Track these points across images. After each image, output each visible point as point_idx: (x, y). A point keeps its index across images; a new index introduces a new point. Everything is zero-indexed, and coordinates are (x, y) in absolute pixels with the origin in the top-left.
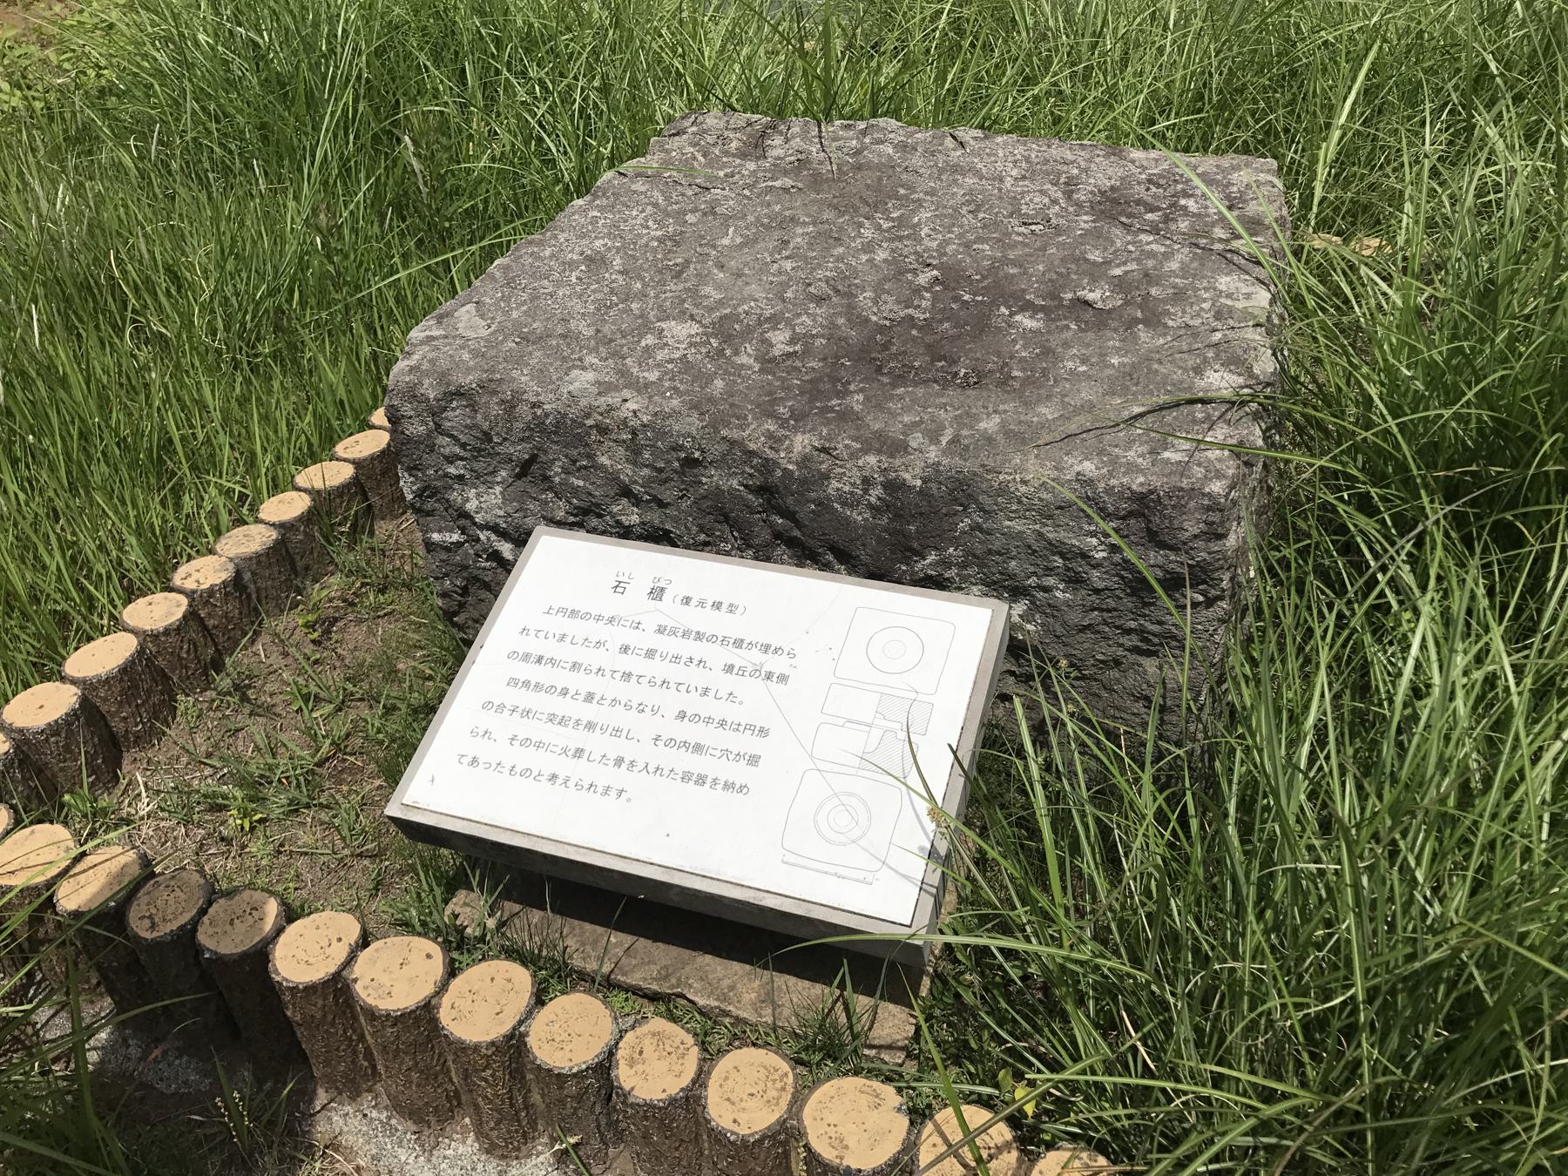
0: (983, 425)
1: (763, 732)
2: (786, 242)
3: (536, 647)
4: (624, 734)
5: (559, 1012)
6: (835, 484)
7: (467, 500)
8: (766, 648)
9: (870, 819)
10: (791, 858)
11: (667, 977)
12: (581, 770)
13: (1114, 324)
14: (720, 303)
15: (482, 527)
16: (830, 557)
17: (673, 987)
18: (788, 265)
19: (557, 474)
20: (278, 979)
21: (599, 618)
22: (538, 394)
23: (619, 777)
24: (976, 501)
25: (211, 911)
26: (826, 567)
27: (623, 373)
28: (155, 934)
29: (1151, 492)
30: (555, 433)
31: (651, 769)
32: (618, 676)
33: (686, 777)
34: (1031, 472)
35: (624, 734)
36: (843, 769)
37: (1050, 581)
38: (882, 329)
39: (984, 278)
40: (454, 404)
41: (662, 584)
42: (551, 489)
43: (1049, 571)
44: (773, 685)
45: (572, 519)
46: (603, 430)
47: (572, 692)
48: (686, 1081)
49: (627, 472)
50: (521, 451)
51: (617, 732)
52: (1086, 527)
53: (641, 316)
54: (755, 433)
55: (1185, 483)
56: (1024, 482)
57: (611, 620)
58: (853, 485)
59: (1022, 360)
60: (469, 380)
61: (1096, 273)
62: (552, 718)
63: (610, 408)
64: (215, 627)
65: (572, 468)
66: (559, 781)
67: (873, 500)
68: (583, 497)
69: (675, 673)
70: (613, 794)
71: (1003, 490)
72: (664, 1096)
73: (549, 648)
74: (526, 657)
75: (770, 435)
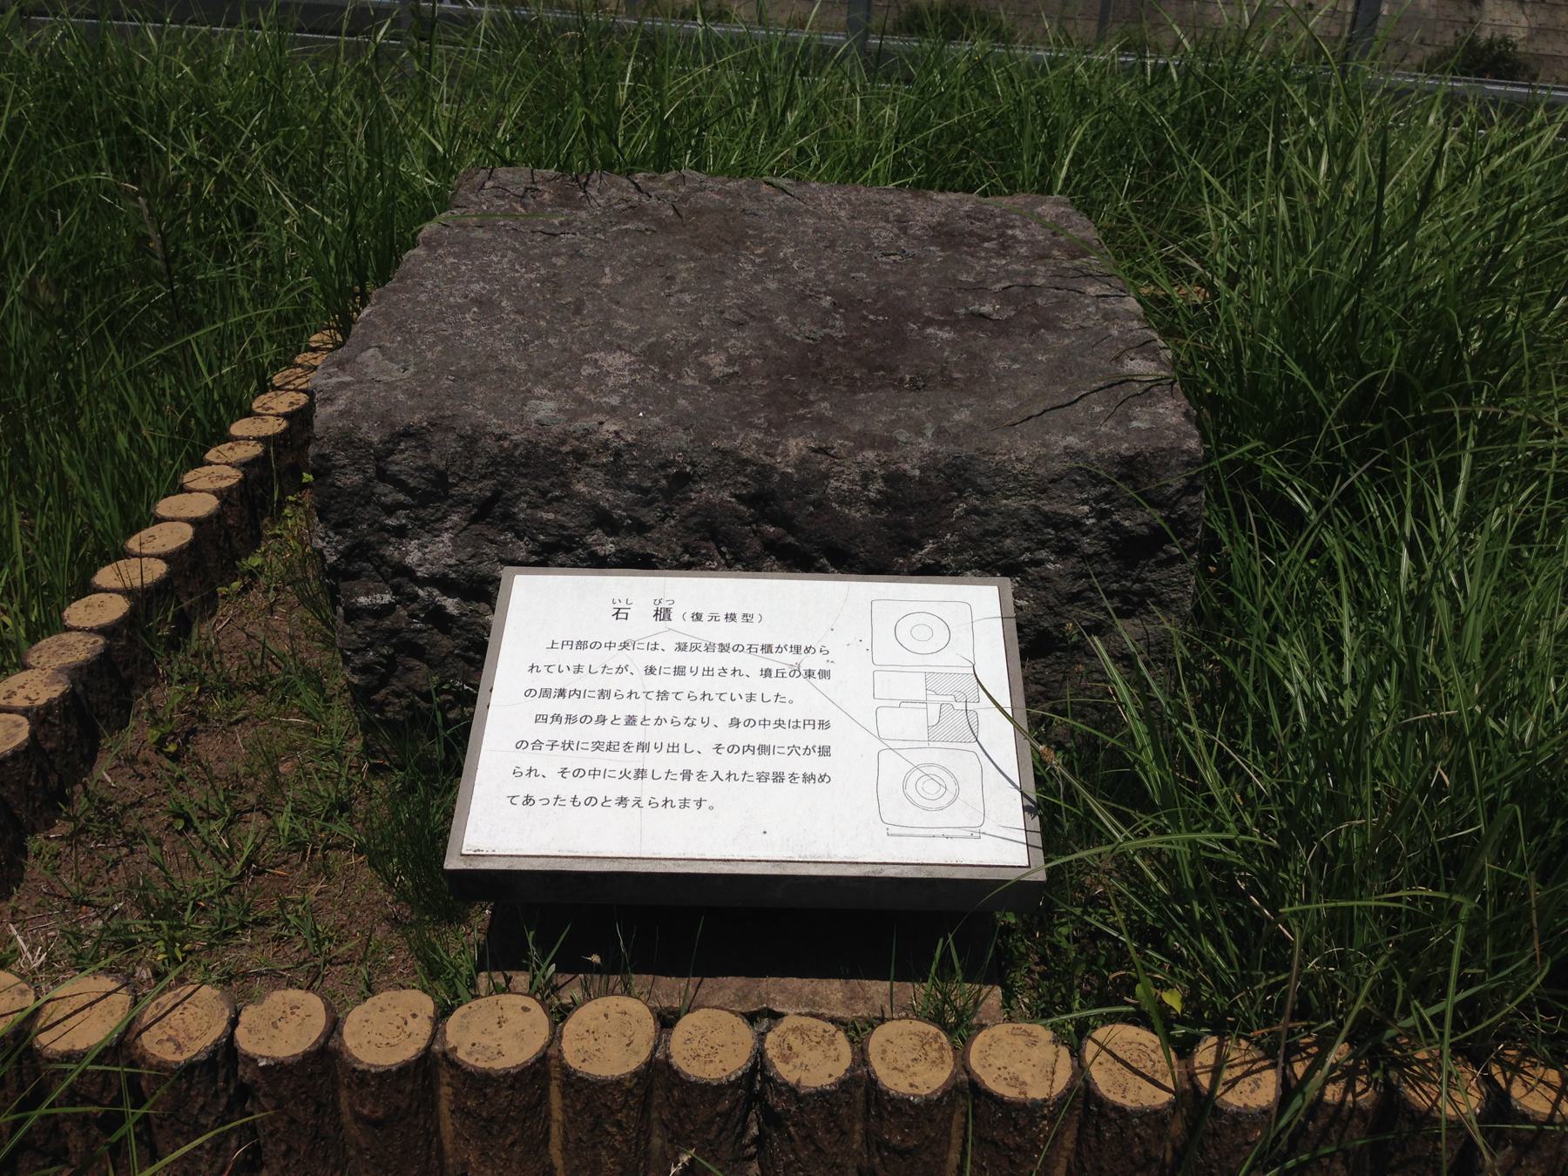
0: (956, 417)
1: (824, 725)
2: (671, 278)
3: (554, 681)
4: (682, 748)
5: (690, 1028)
6: (834, 483)
7: (407, 553)
8: (797, 649)
9: (957, 783)
10: (894, 830)
11: (745, 997)
12: (646, 789)
13: (1018, 331)
14: (641, 334)
15: (422, 583)
16: (824, 561)
17: (755, 1004)
18: (687, 298)
19: (523, 510)
20: (365, 1067)
21: (610, 645)
22: (500, 427)
23: (692, 789)
24: (973, 484)
25: (243, 1018)
26: (822, 570)
27: (581, 400)
28: (187, 1055)
29: (1138, 454)
30: (525, 465)
31: (723, 775)
32: (653, 696)
33: (762, 777)
34: (1020, 450)
35: (682, 748)
36: (916, 744)
37: (1043, 554)
38: (810, 348)
39: (876, 301)
40: (403, 446)
41: (665, 605)
42: (510, 528)
43: (1043, 544)
44: (817, 681)
45: (534, 558)
46: (580, 456)
47: (610, 718)
48: (846, 1061)
49: (607, 497)
50: (485, 488)
51: (673, 748)
52: (1078, 496)
53: (565, 350)
54: (747, 442)
55: (1164, 444)
56: (1020, 460)
57: (625, 645)
58: (852, 482)
59: (956, 364)
60: (417, 418)
61: (979, 289)
62: (598, 746)
63: (587, 432)
64: (53, 751)
65: (545, 499)
66: (630, 804)
67: (872, 495)
68: (553, 531)
69: (714, 685)
70: (692, 805)
71: (999, 470)
72: (832, 1080)
73: (568, 681)
74: (546, 693)
75: (759, 443)
